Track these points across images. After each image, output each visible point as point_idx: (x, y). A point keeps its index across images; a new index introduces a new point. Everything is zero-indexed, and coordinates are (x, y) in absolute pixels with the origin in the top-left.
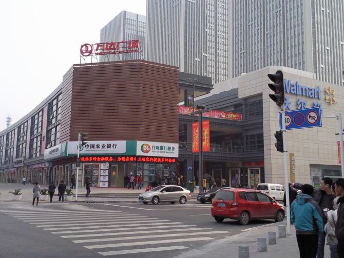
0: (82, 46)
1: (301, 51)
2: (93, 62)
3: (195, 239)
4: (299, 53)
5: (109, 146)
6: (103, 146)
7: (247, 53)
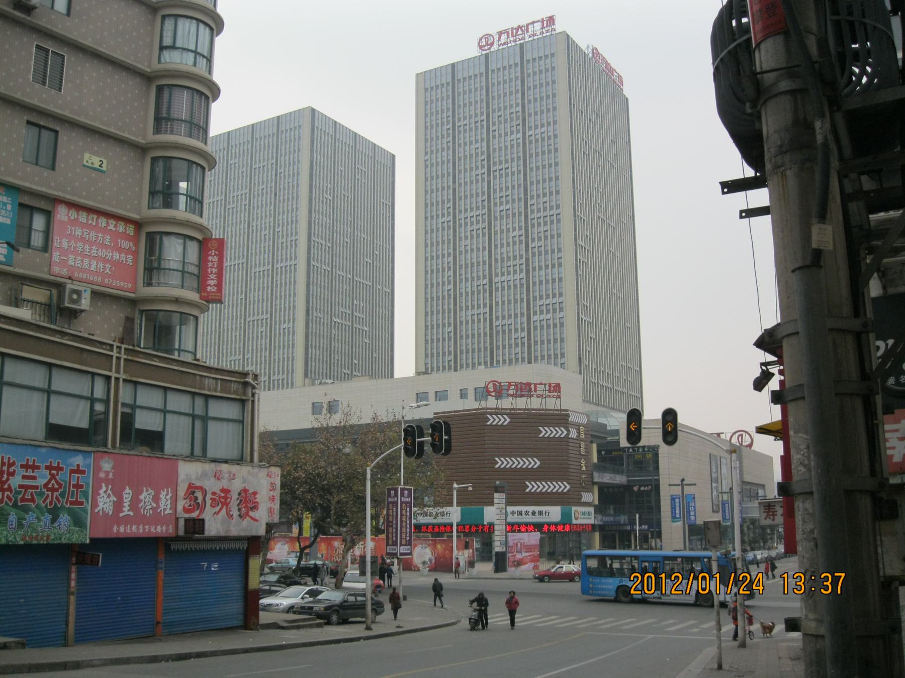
0: (481, 39)
1: (295, 195)
2: (764, 69)
3: (568, 619)
4: (293, 197)
5: (541, 513)
6: (534, 513)
7: (271, 320)
